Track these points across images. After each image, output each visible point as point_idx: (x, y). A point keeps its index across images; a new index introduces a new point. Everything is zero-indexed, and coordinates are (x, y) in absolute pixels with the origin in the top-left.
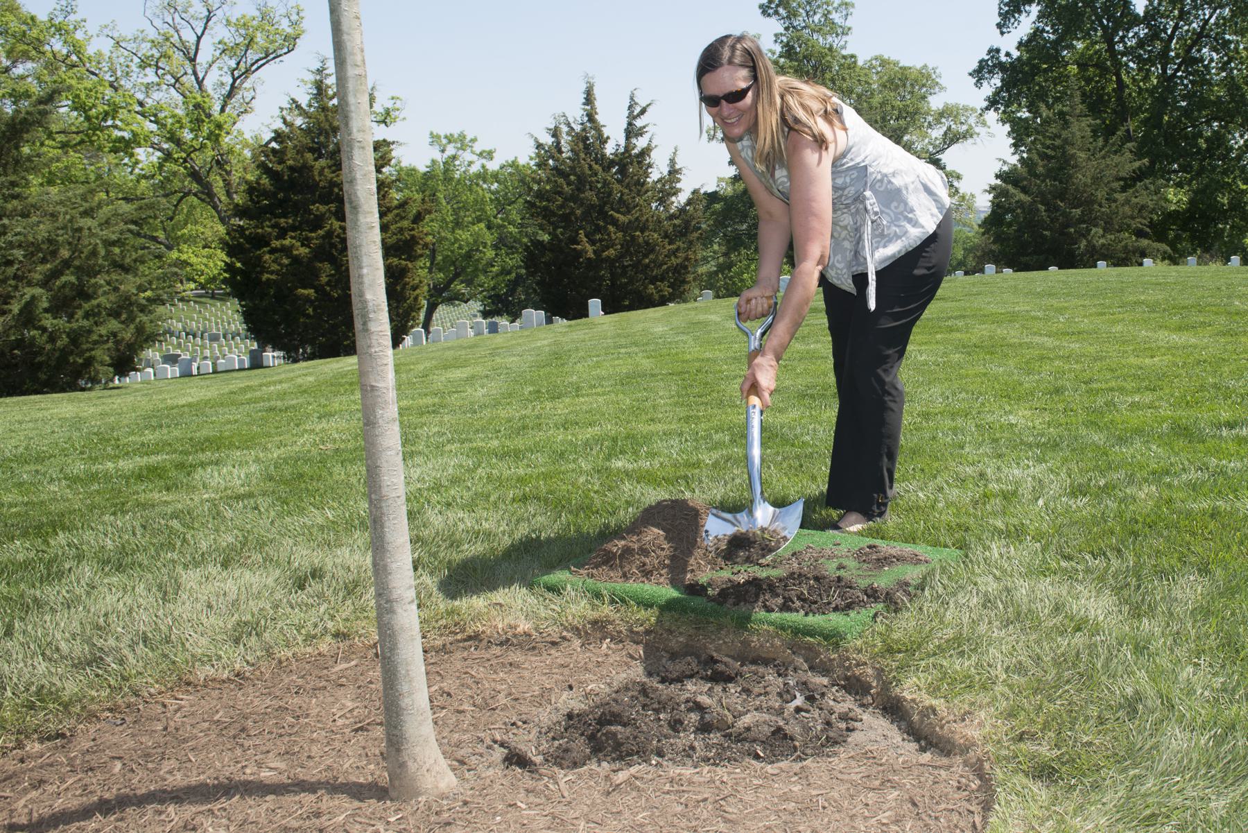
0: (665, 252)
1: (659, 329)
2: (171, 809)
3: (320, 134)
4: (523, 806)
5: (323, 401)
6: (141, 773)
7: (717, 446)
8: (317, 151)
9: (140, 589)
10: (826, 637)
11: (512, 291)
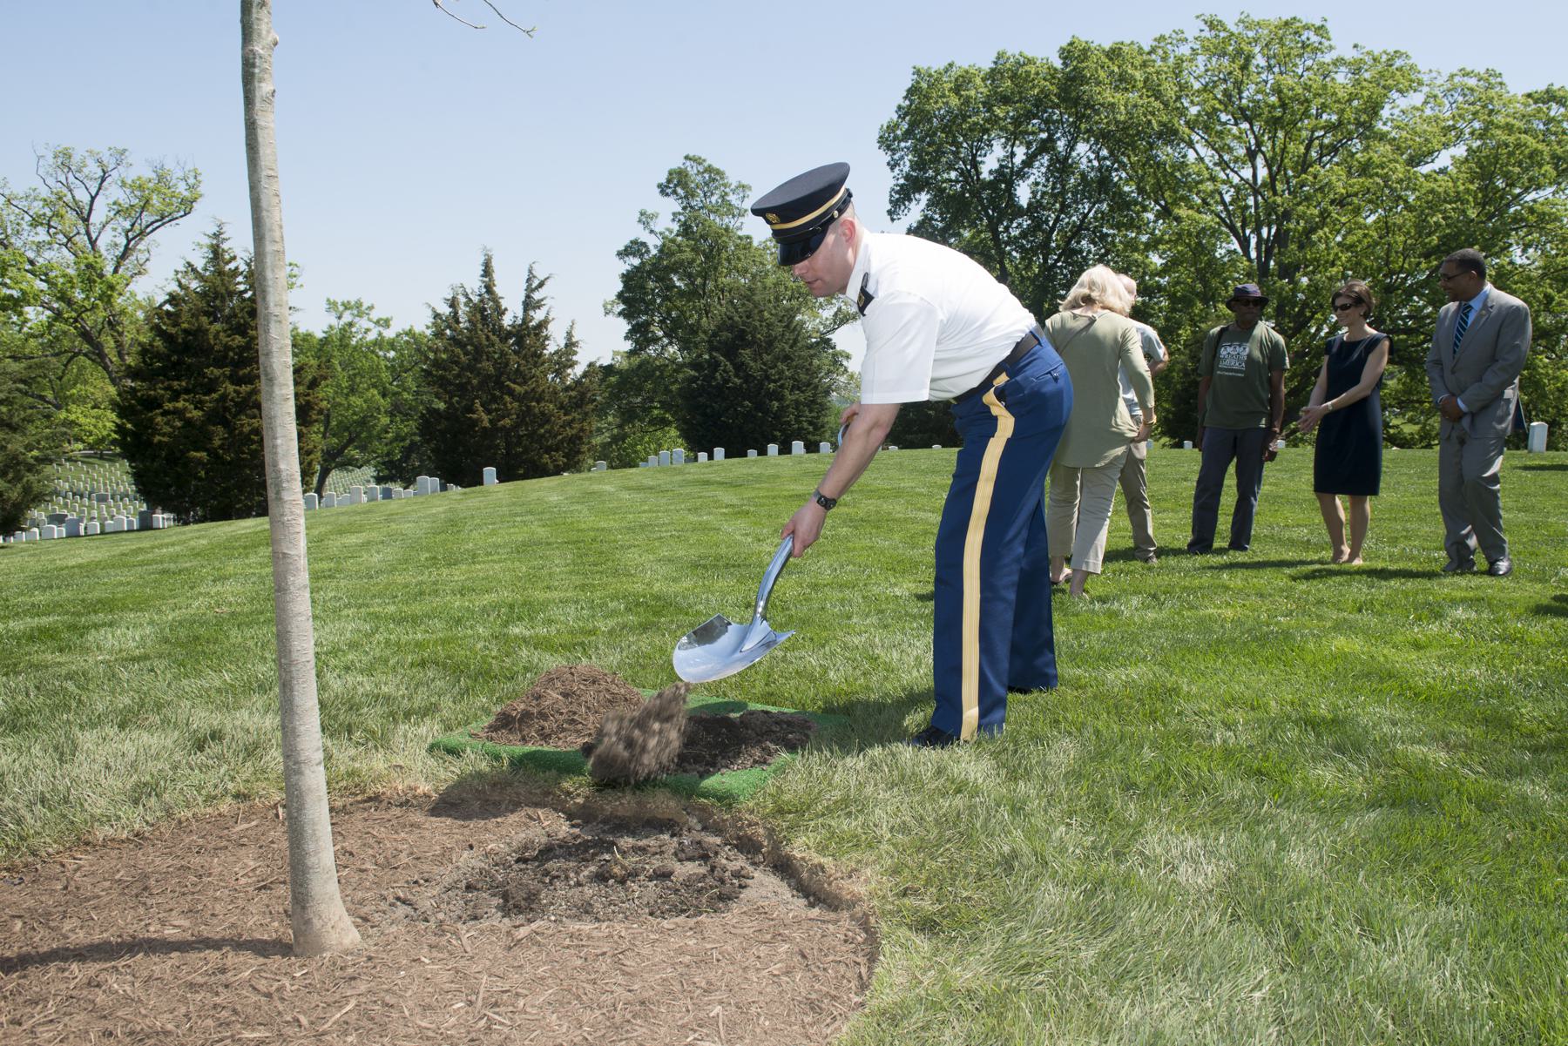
0: (560, 422)
1: (554, 498)
2: (74, 966)
5: (217, 564)
6: (42, 932)
7: (613, 613)
8: (212, 314)
10: (720, 799)
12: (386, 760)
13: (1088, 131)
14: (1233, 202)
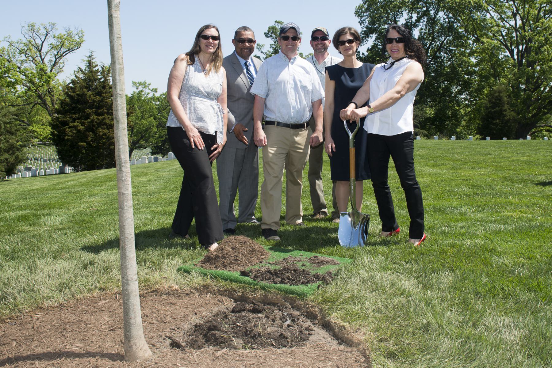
3: (90, 81)
4: (179, 365)
6: (24, 347)
8: (88, 88)
9: (21, 268)
10: (299, 295)
11: (163, 145)
12: (160, 275)
13: (443, 7)
14: (506, 35)
